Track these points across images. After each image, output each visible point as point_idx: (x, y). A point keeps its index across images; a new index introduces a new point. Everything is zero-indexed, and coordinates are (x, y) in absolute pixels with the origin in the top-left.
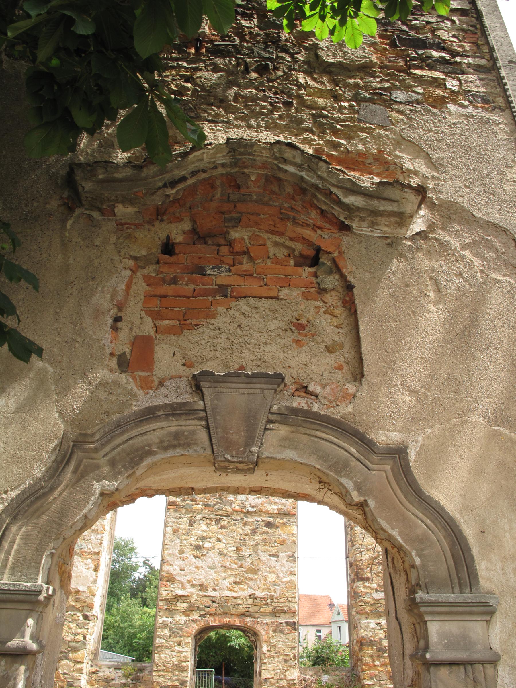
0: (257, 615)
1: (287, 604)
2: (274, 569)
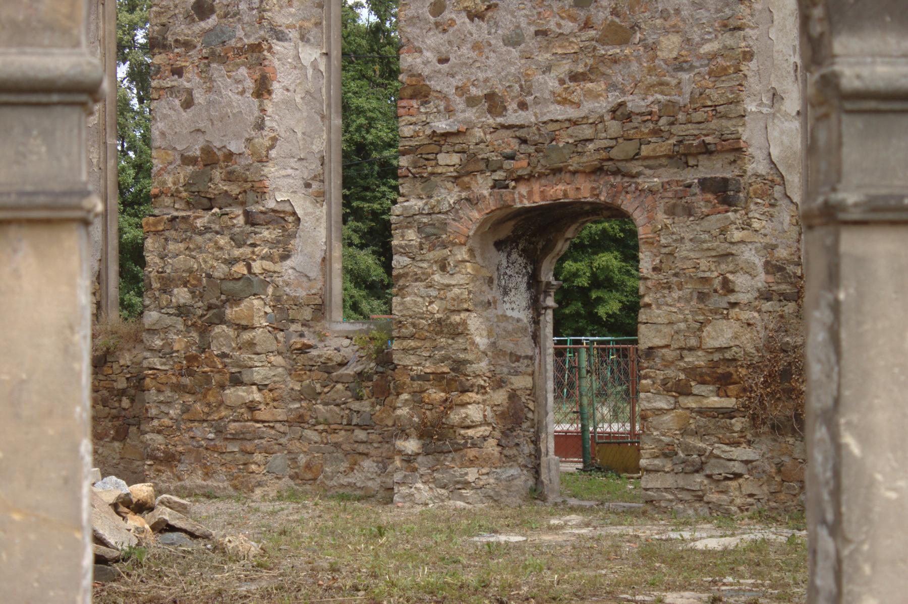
0: (635, 167)
1: (714, 124)
2: (673, 20)
